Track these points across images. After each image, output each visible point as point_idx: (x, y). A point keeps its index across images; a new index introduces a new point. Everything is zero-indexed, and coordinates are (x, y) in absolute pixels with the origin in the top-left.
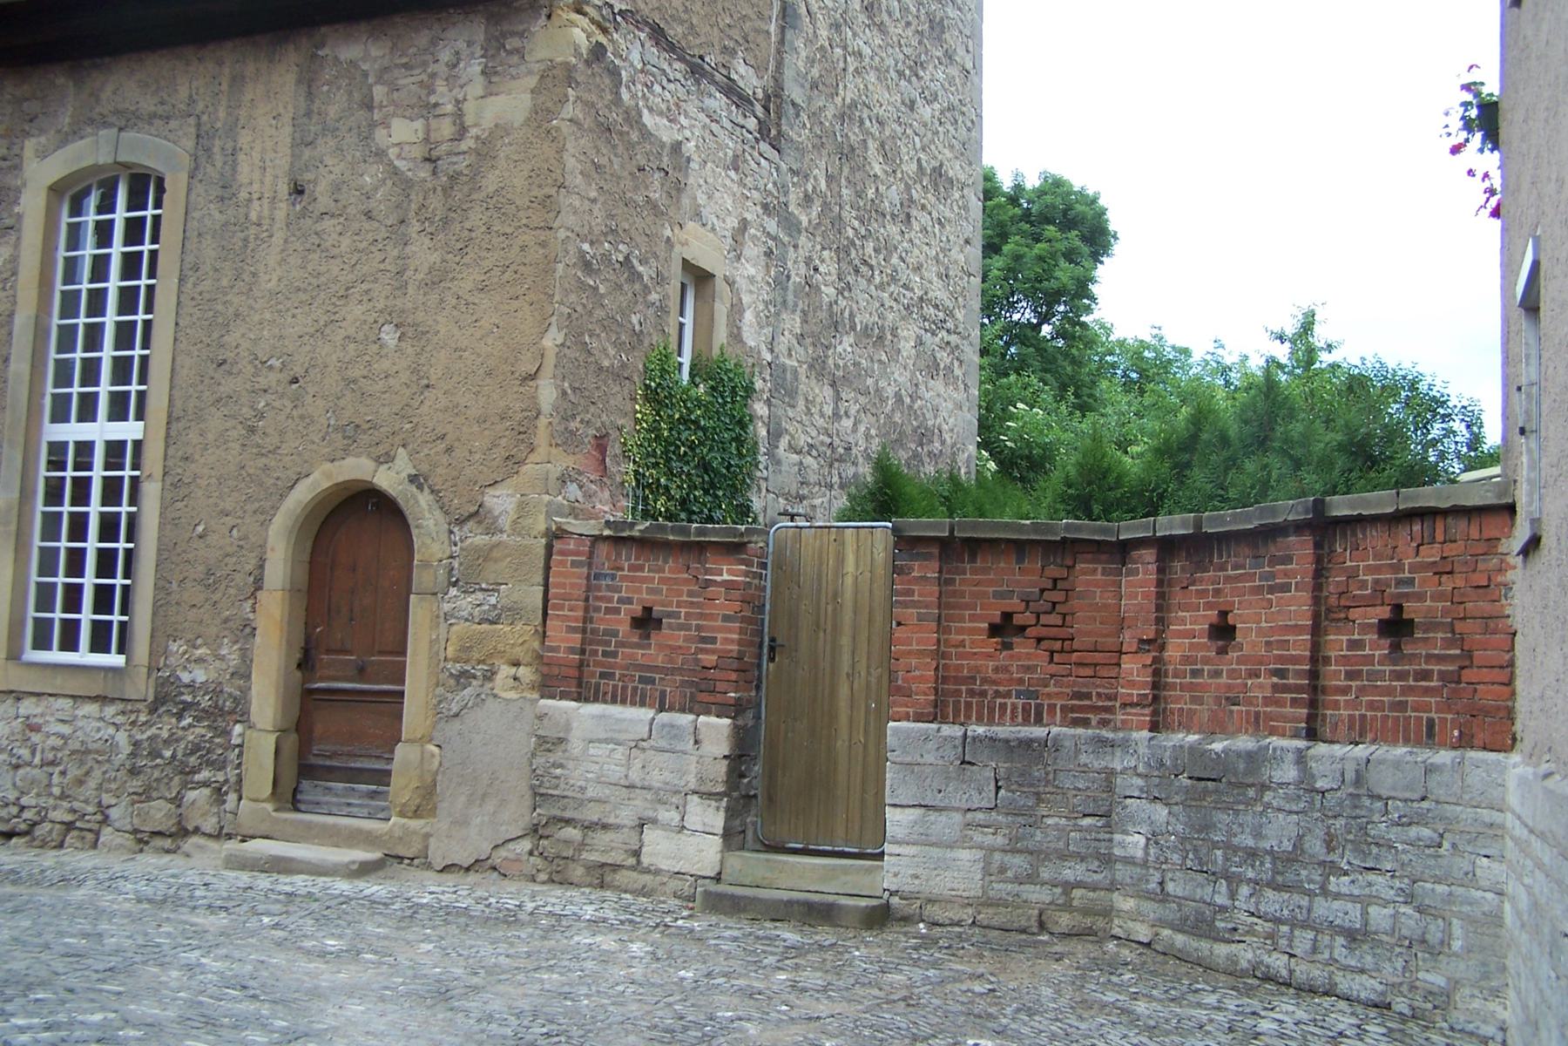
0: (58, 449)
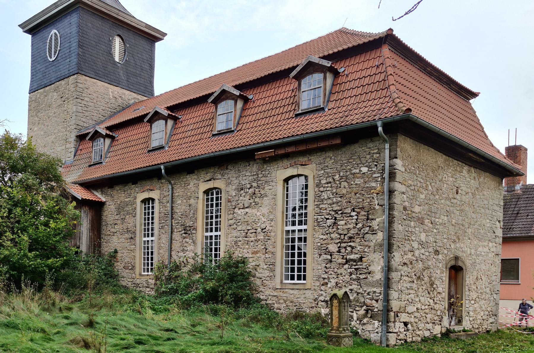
0: (145, 241)
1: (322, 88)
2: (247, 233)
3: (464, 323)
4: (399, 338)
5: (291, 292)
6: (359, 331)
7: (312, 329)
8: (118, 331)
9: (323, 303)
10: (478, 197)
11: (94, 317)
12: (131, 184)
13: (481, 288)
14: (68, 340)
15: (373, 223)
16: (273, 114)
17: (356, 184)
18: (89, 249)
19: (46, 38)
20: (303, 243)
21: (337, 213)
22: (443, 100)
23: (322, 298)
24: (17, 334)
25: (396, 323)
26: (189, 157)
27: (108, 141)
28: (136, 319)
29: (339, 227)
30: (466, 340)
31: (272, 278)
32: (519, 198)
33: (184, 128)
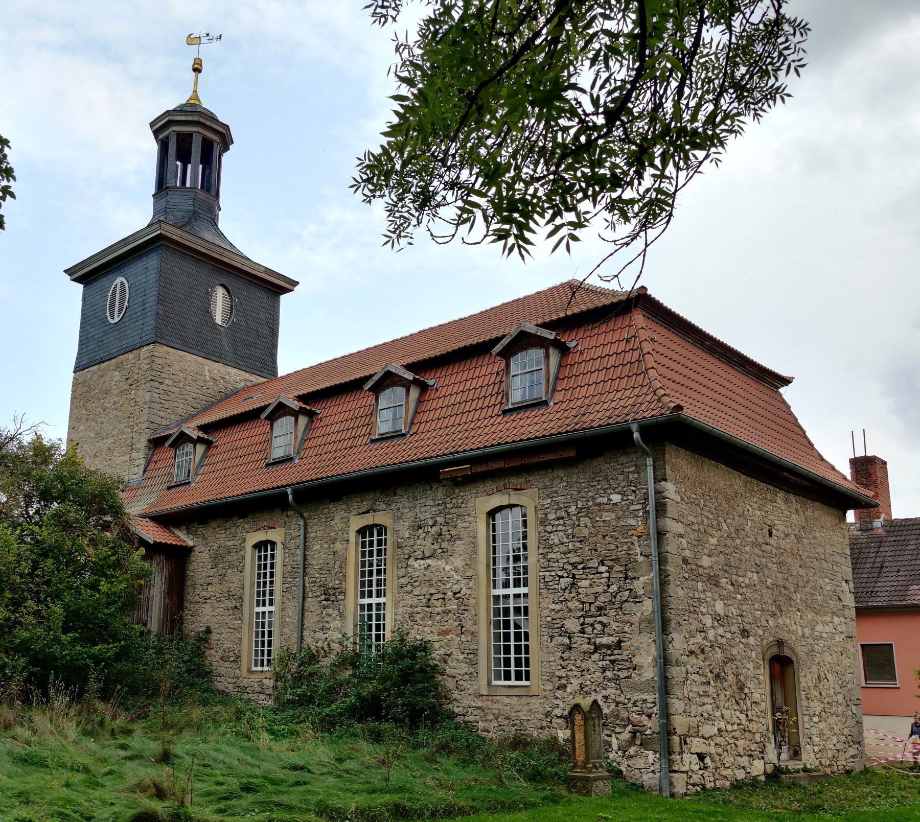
0: (258, 613)
1: (543, 371)
2: (429, 600)
3: (804, 756)
4: (692, 781)
5: (506, 700)
6: (623, 768)
7: (540, 765)
8: (212, 769)
9: (560, 721)
10: (806, 541)
11: (171, 747)
12: (237, 517)
13: (828, 695)
14: (127, 785)
15: (635, 584)
16: (467, 408)
17: (604, 521)
18: (163, 626)
19: (107, 290)
20: (522, 617)
21: (576, 568)
22: (735, 389)
23: (558, 712)
24: (42, 775)
25: (684, 755)
26: (333, 476)
27: (200, 449)
28: (242, 748)
29: (580, 590)
30: (808, 786)
31: (473, 675)
32: (881, 542)
33: (324, 429)
